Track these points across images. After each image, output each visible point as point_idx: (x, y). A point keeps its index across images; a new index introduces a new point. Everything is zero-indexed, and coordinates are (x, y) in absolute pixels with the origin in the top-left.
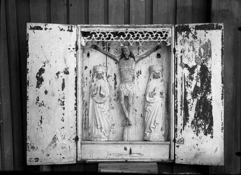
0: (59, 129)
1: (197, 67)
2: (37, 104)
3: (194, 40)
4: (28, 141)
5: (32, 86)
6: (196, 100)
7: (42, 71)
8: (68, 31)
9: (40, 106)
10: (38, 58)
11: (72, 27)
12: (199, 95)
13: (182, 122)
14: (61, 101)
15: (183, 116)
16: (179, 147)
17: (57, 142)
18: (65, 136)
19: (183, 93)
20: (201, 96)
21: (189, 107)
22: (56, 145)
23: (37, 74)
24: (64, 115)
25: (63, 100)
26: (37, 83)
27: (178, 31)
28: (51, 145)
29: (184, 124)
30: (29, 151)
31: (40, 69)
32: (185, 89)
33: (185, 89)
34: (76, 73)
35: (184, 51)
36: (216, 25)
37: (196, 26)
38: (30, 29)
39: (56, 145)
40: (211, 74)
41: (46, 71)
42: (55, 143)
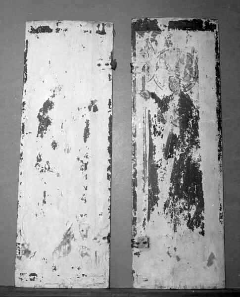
0: (76, 217)
1: (172, 99)
2: (37, 166)
3: (167, 48)
4: (19, 240)
5: (30, 133)
6: (171, 161)
7: (48, 105)
8: (97, 32)
9: (42, 171)
10: (43, 82)
11: (103, 25)
12: (177, 152)
13: (145, 205)
14: (82, 161)
15: (147, 192)
16: (140, 256)
17: (72, 242)
18: (89, 232)
19: (148, 148)
20: (181, 153)
21: (160, 175)
22: (70, 249)
23: (41, 111)
24: (86, 189)
25: (85, 161)
26: (39, 128)
27: (138, 30)
28: (61, 248)
29: (151, 209)
30: (20, 258)
31: (45, 102)
32: (151, 140)
33: (151, 140)
34: (111, 110)
35: (148, 68)
36: (207, 23)
37: (170, 22)
38: (31, 32)
39: (69, 248)
40: (198, 112)
41: (55, 106)
42: (68, 245)
